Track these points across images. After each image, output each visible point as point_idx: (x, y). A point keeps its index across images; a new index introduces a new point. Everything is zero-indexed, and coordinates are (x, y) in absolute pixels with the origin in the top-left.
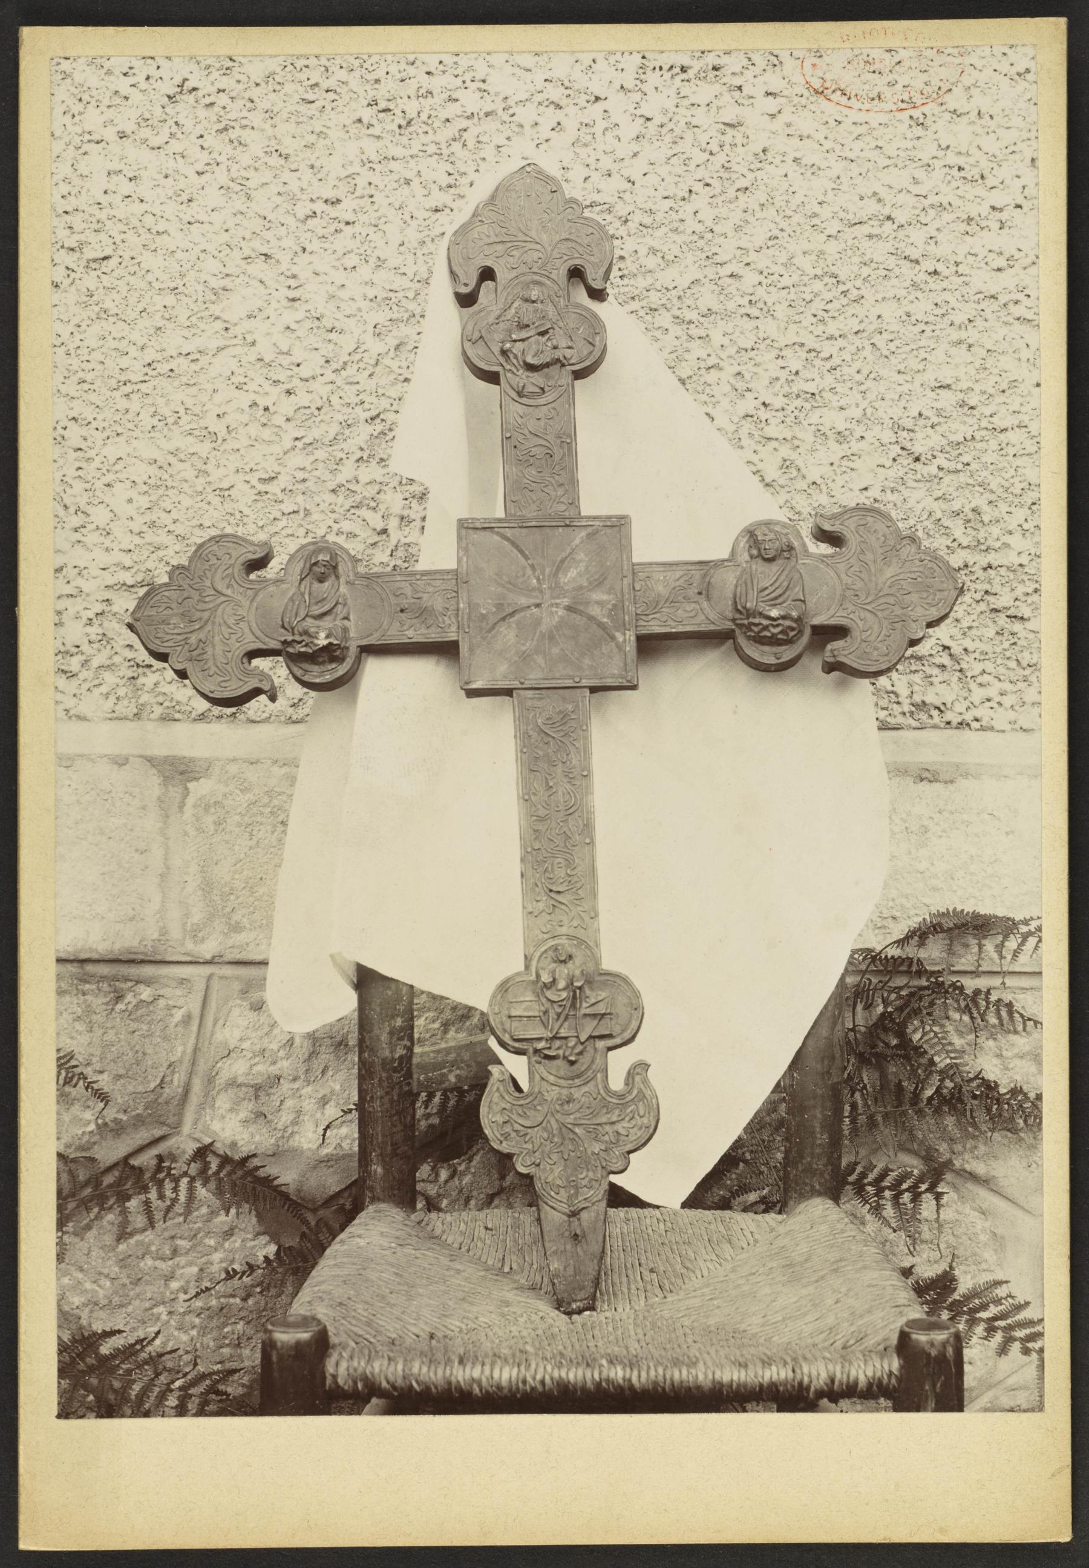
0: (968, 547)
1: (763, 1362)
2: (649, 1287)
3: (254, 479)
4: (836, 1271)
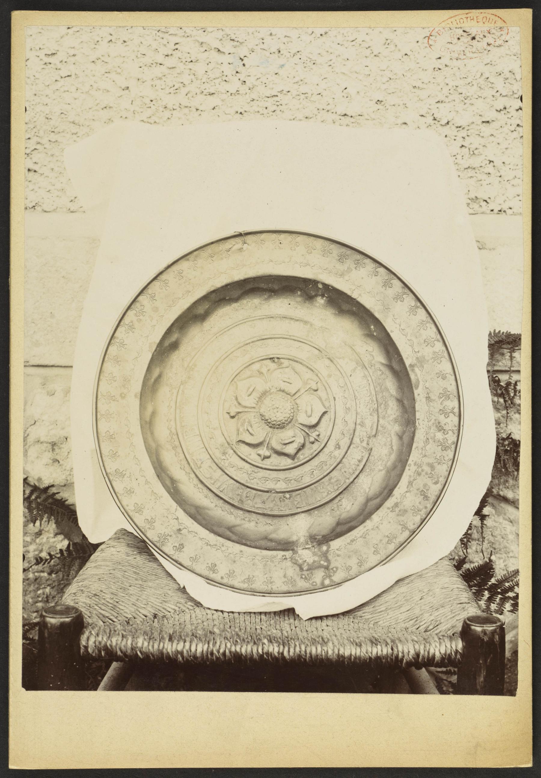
0: (506, 96)
1: (372, 642)
3: (42, 54)
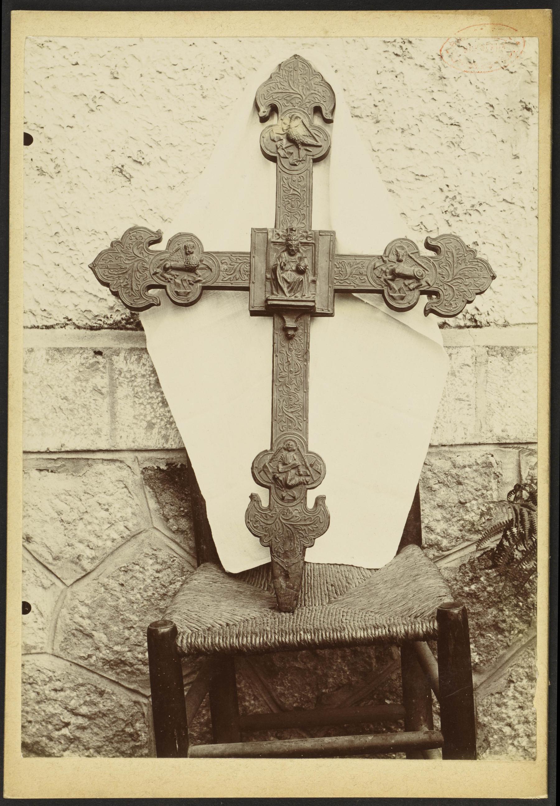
1: (375, 627)
2: (331, 593)
4: (414, 580)
